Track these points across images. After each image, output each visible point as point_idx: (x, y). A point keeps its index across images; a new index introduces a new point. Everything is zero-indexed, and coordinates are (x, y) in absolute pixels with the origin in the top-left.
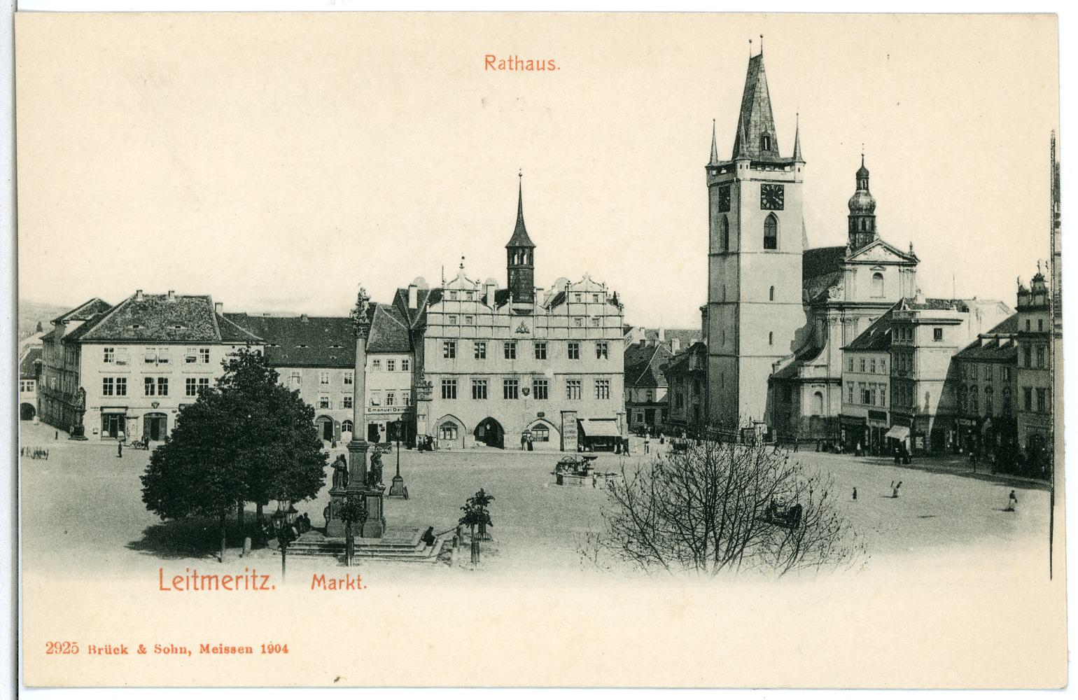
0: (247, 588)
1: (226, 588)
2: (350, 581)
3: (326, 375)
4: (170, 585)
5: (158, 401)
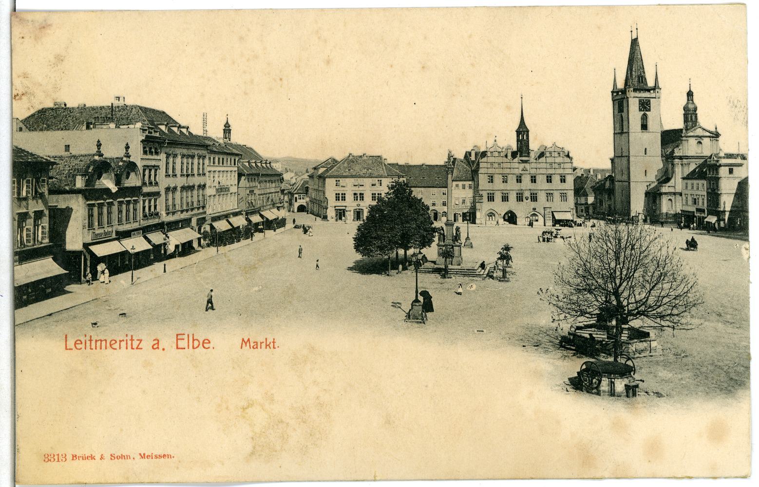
1: (111, 347)
2: (268, 343)
4: (72, 346)
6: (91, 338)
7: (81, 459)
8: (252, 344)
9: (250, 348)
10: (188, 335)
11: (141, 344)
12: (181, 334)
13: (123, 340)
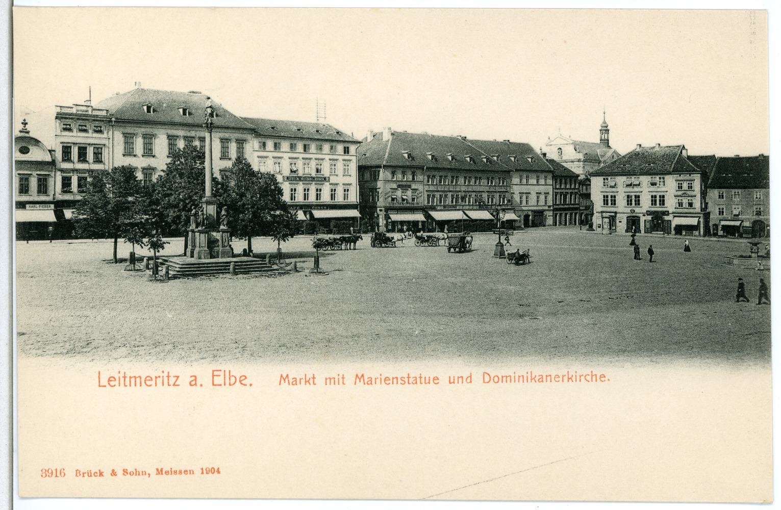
1: (242, 384)
2: (307, 379)
3: (758, 194)
4: (106, 384)
5: (634, 209)
7: (86, 475)
11: (178, 381)
12: (217, 371)
13: (159, 377)
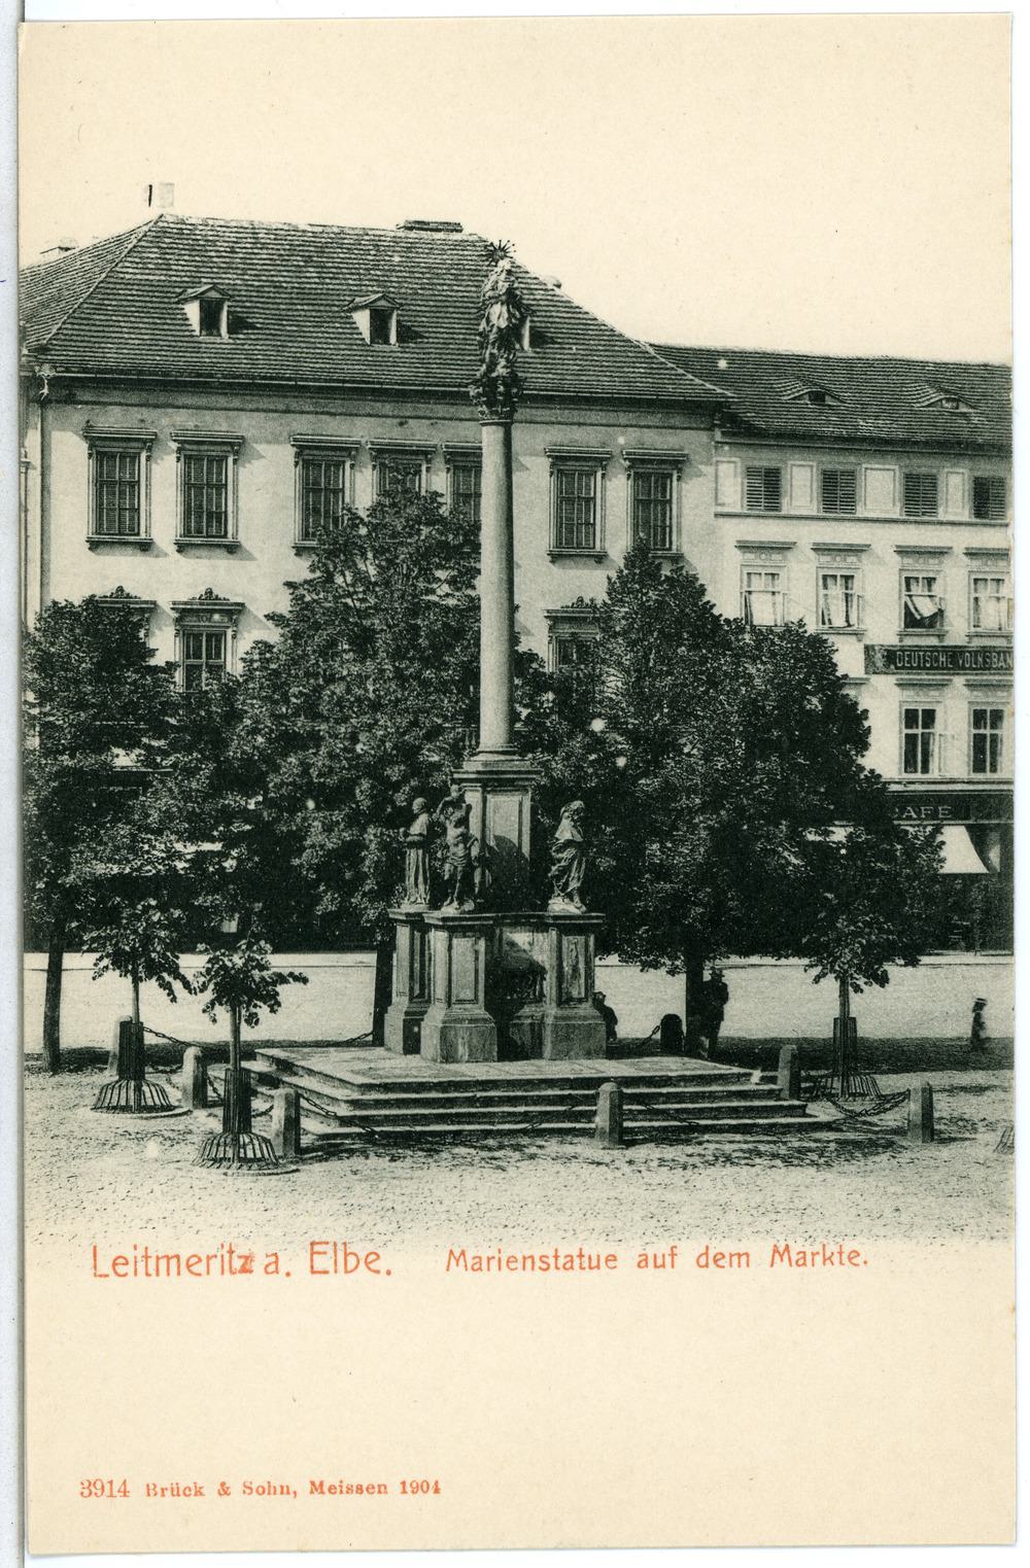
0: (500, 1269)
1: (192, 1272)
2: (828, 1254)
6: (146, 1252)
8: (794, 1258)
9: (791, 1265)
10: (335, 1244)
